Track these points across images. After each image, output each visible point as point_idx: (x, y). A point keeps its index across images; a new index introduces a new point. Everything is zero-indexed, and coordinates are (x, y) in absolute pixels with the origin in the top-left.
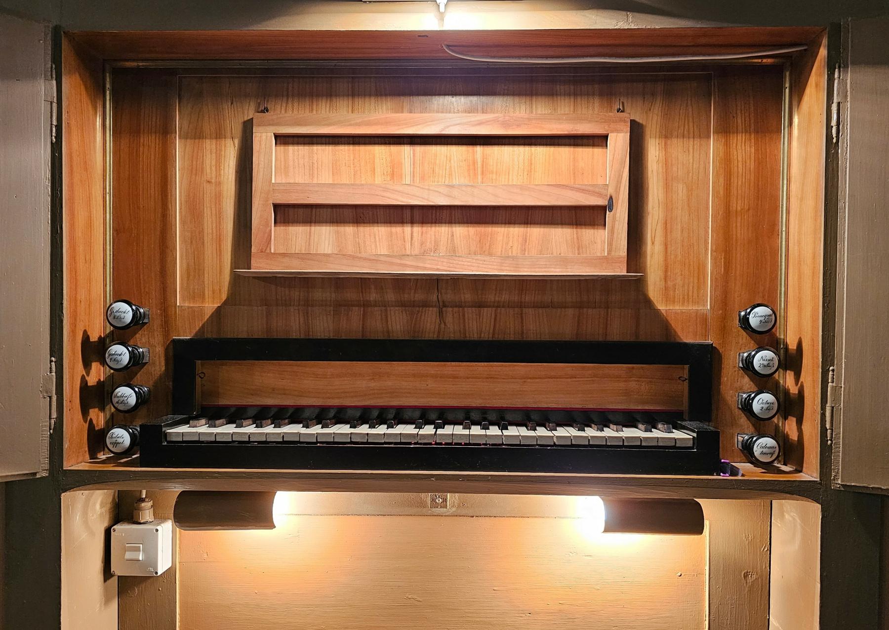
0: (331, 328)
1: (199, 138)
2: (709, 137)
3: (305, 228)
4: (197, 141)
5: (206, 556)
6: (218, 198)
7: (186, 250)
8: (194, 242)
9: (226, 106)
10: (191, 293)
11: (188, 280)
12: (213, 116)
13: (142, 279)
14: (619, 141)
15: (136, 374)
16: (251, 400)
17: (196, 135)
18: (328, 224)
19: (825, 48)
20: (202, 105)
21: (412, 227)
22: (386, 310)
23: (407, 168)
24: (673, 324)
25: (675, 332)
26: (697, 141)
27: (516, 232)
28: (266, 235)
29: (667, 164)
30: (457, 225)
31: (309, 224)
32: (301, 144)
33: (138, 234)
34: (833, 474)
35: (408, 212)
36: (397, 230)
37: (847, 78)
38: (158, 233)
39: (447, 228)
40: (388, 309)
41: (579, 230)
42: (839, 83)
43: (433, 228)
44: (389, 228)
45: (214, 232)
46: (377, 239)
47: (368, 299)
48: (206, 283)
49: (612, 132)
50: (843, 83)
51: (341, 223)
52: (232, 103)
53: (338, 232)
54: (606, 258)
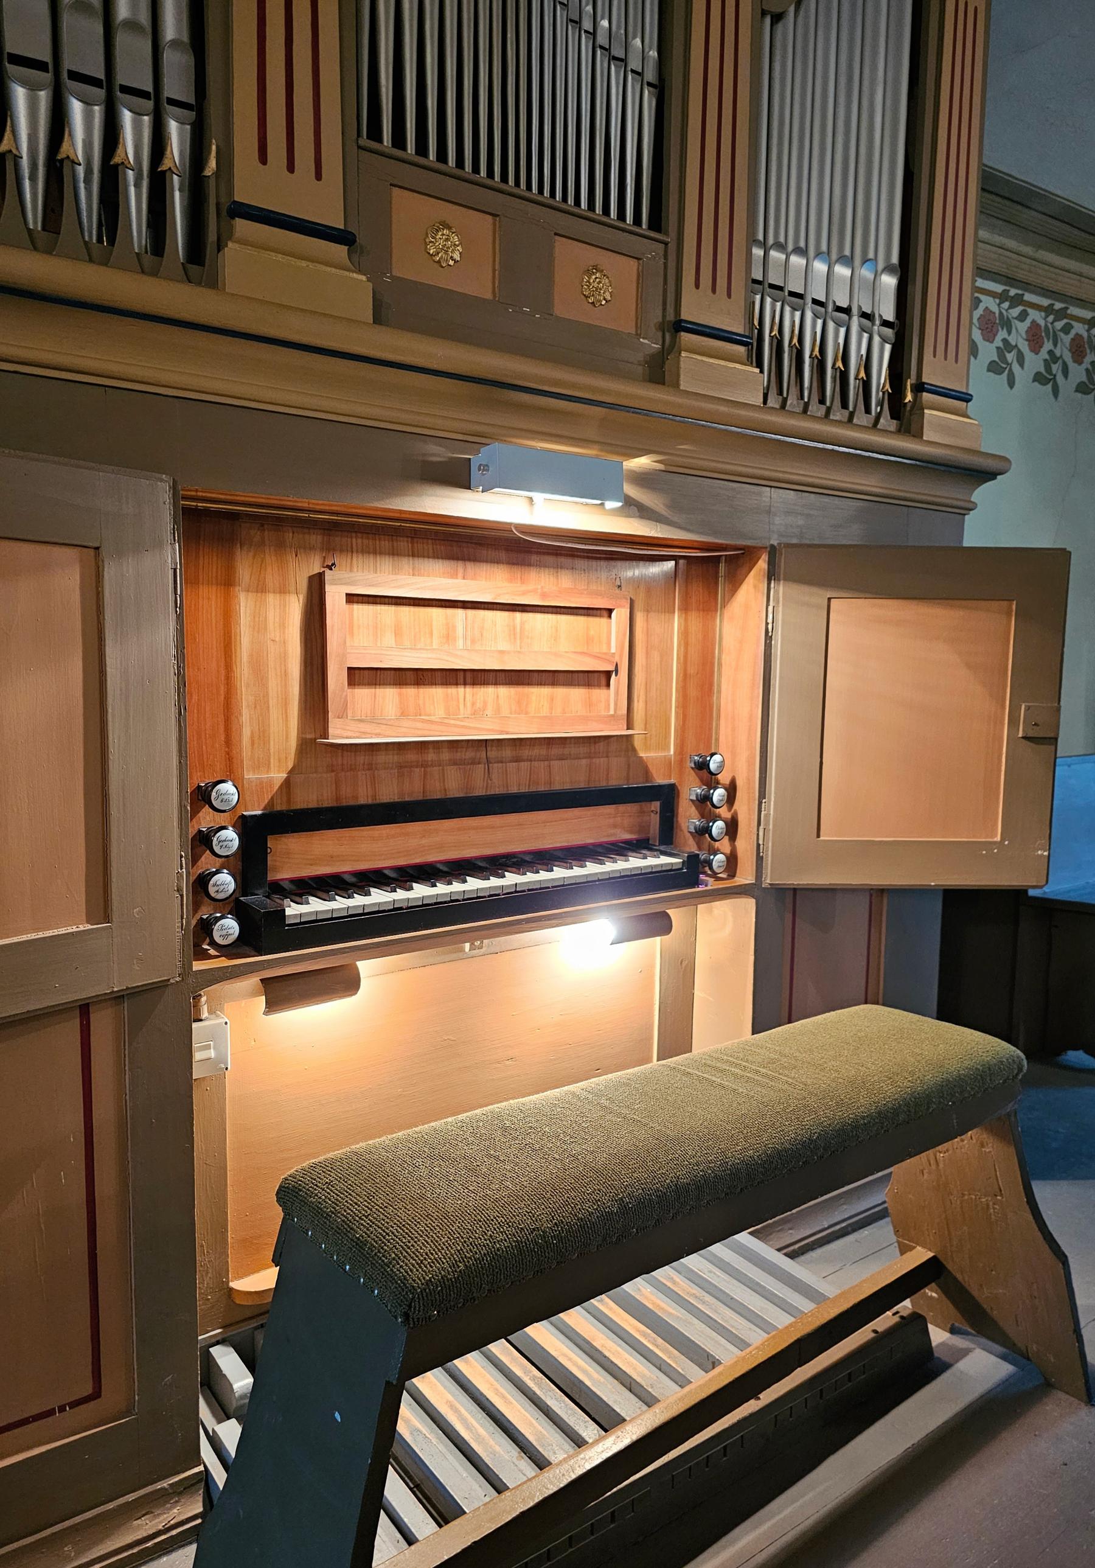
0: (396, 792)
1: (262, 592)
2: (674, 612)
3: (371, 690)
4: (259, 594)
5: (253, 1043)
6: (284, 657)
7: (250, 714)
8: (258, 707)
9: (291, 558)
10: (256, 763)
11: (252, 749)
12: (276, 569)
13: (204, 752)
14: (620, 615)
15: (201, 857)
16: (309, 871)
17: (261, 589)
18: (392, 686)
19: (765, 561)
20: (265, 555)
21: (465, 688)
22: (443, 770)
23: (460, 630)
24: (650, 767)
25: (652, 775)
26: (667, 614)
27: (545, 691)
28: (343, 700)
29: (648, 633)
30: (501, 686)
31: (374, 687)
32: (365, 603)
33: (198, 700)
34: (764, 876)
35: (462, 673)
36: (452, 691)
37: (780, 589)
38: (222, 697)
39: (493, 689)
40: (445, 768)
41: (590, 690)
42: (774, 592)
43: (482, 689)
44: (445, 689)
45: (280, 695)
46: (435, 700)
47: (426, 759)
48: (272, 751)
49: (618, 607)
50: (777, 592)
51: (403, 685)
52: (296, 556)
53: (400, 694)
54: (612, 716)
